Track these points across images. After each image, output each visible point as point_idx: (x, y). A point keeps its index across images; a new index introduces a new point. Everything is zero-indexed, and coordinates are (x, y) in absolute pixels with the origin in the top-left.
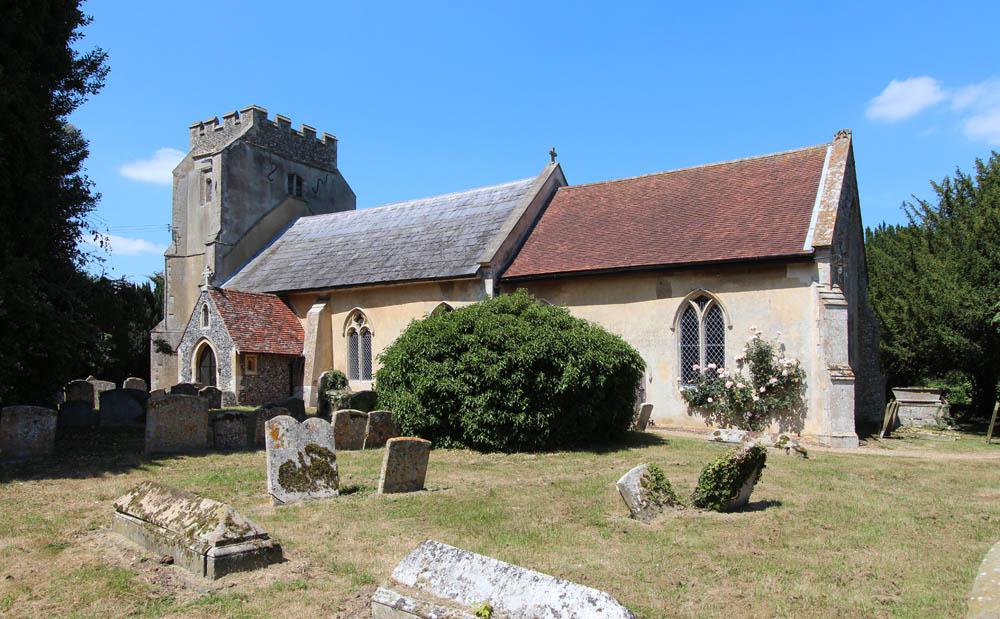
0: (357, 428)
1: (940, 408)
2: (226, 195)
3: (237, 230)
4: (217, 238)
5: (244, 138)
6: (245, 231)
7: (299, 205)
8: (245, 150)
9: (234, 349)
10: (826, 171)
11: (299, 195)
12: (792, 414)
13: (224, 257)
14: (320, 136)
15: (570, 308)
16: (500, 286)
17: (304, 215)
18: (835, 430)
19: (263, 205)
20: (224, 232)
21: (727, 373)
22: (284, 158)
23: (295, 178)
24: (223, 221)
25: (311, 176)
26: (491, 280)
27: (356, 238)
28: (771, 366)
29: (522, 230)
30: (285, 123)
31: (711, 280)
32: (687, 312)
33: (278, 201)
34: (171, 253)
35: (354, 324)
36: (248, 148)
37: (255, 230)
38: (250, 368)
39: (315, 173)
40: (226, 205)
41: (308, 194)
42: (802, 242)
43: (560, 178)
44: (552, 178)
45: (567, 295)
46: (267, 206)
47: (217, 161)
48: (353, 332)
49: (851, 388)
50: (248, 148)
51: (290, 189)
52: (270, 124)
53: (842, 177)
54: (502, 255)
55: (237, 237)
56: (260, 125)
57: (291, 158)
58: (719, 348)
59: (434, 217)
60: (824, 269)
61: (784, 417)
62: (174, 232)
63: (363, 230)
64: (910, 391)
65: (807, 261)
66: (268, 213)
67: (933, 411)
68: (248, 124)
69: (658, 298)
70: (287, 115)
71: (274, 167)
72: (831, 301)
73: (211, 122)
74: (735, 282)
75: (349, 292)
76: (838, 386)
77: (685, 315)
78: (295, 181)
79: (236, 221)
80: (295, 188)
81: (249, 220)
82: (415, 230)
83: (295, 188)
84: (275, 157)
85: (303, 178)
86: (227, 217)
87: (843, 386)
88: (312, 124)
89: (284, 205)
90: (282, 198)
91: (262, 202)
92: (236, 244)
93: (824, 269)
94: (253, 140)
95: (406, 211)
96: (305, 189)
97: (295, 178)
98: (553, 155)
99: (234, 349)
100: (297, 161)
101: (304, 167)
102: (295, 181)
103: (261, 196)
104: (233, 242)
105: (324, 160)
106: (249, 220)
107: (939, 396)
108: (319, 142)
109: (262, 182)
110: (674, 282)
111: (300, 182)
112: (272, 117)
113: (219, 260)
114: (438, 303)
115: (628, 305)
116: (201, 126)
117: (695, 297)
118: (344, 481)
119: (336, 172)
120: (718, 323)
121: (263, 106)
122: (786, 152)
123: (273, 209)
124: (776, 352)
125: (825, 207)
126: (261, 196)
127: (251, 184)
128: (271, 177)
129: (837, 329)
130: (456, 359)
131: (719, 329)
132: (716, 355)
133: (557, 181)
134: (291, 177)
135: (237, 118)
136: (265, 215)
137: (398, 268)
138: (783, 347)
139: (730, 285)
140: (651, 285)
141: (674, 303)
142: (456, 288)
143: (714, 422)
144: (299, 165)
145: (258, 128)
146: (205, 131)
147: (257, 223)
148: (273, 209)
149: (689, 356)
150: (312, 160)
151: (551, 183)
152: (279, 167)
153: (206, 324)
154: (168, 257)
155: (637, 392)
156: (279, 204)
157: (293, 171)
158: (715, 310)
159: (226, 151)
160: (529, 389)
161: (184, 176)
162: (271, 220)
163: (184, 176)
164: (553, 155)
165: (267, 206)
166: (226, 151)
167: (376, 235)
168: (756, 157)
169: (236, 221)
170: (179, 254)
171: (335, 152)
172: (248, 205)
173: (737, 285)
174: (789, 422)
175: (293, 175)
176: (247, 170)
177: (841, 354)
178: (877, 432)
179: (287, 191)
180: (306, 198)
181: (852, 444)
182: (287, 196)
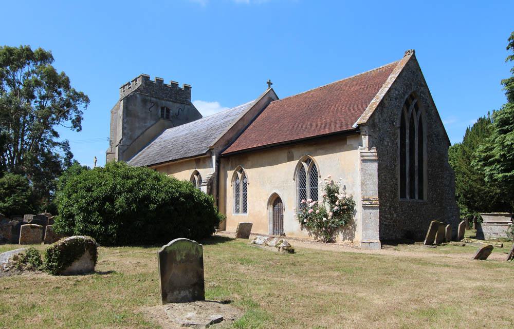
0: (36, 234)
1: (510, 226)
2: (125, 120)
3: (131, 138)
4: (120, 143)
5: (136, 91)
7: (166, 123)
8: (136, 97)
11: (168, 118)
12: (349, 229)
14: (181, 86)
17: (170, 127)
18: (365, 238)
19: (146, 124)
20: (124, 140)
22: (159, 99)
23: (165, 108)
24: (123, 134)
25: (174, 108)
26: (215, 156)
29: (240, 127)
30: (160, 81)
31: (311, 149)
32: (300, 168)
33: (154, 122)
34: (108, 152)
36: (138, 96)
37: (141, 137)
39: (177, 105)
40: (125, 125)
41: (172, 117)
43: (273, 97)
44: (267, 96)
45: (249, 163)
46: (148, 124)
49: (377, 212)
50: (138, 96)
51: (162, 115)
52: (152, 82)
54: (223, 142)
55: (131, 141)
56: (146, 84)
57: (163, 99)
60: (365, 140)
61: (345, 231)
62: (111, 141)
64: (488, 215)
65: (356, 133)
66: (149, 128)
67: (505, 228)
69: (288, 161)
70: (160, 76)
71: (153, 104)
72: (366, 158)
73: (127, 85)
74: (322, 149)
75: (162, 167)
76: (368, 211)
77: (301, 170)
79: (130, 133)
84: (154, 99)
86: (125, 131)
87: (371, 211)
88: (176, 80)
89: (158, 124)
90: (157, 120)
91: (145, 123)
92: (130, 145)
93: (365, 140)
94: (141, 91)
96: (171, 115)
97: (165, 108)
98: (270, 84)
100: (167, 100)
101: (171, 103)
103: (145, 119)
104: (129, 144)
105: (183, 98)
106: (138, 132)
107: (510, 218)
108: (180, 89)
109: (146, 112)
110: (295, 152)
111: (168, 111)
112: (153, 79)
113: (120, 154)
114: (194, 170)
115: (274, 166)
116: (124, 87)
117: (305, 159)
121: (147, 73)
122: (379, 68)
123: (152, 126)
124: (341, 190)
126: (145, 119)
127: (139, 114)
129: (370, 175)
132: (315, 196)
133: (271, 97)
134: (163, 109)
136: (146, 130)
138: (345, 188)
139: (321, 151)
140: (284, 154)
141: (295, 163)
142: (201, 162)
143: (312, 234)
144: (168, 102)
145: (144, 85)
147: (142, 134)
149: (303, 195)
151: (266, 100)
152: (156, 104)
154: (108, 154)
156: (155, 123)
157: (164, 105)
158: (313, 168)
160: (102, 211)
161: (115, 113)
162: (150, 132)
163: (115, 113)
164: (270, 84)
165: (148, 124)
168: (363, 73)
169: (130, 133)
170: (112, 152)
173: (323, 151)
174: (348, 234)
175: (164, 107)
176: (137, 107)
177: (373, 191)
178: (422, 240)
179: (160, 116)
180: (171, 119)
181: (377, 249)
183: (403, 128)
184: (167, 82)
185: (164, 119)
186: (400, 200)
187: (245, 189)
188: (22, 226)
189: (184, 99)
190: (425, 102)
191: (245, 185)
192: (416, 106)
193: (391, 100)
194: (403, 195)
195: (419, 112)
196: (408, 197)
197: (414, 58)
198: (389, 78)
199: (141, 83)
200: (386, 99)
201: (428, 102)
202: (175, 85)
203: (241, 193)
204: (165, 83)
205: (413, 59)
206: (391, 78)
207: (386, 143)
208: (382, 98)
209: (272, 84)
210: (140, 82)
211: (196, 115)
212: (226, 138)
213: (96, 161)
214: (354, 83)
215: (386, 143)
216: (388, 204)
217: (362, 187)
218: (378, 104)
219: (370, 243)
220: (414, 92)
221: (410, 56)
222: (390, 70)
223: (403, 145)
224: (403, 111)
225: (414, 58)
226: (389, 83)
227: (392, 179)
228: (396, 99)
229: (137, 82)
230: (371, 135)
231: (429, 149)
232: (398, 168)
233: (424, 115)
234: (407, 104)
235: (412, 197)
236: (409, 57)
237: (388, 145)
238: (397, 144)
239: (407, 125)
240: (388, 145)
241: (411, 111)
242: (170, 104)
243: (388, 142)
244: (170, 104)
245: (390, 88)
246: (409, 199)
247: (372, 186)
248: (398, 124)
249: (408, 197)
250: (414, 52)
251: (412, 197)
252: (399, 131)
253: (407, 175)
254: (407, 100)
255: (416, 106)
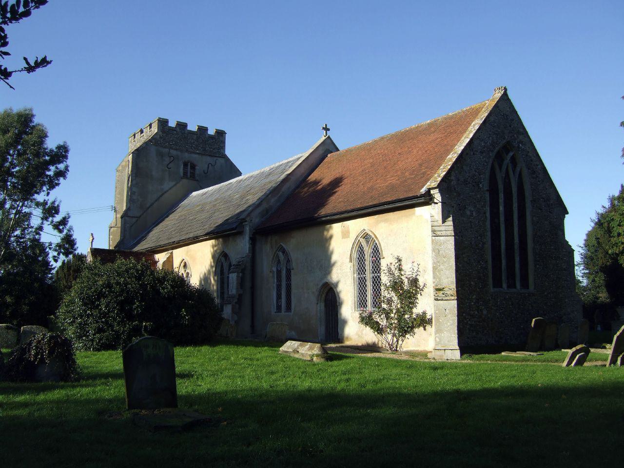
6: (148, 206)
11: (193, 177)
21: (384, 281)
23: (189, 164)
25: (202, 163)
28: (52, 151)
30: (182, 126)
39: (209, 159)
51: (185, 174)
78: (189, 167)
86: (135, 197)
92: (140, 216)
96: (197, 172)
97: (189, 164)
98: (326, 129)
100: (191, 153)
102: (189, 167)
111: (193, 167)
112: (172, 124)
118: (36, 59)
128: (169, 166)
133: (328, 147)
134: (185, 165)
145: (161, 133)
151: (321, 152)
155: (338, 304)
183: (493, 190)
184: (192, 127)
185: (187, 178)
186: (492, 290)
187: (289, 278)
188: (534, 320)
189: (216, 150)
190: (527, 155)
191: (289, 272)
192: (513, 159)
193: (474, 154)
194: (497, 283)
195: (518, 169)
196: (505, 285)
197: (506, 98)
198: (472, 124)
199: (156, 131)
200: (467, 154)
201: (530, 154)
202: (203, 130)
203: (369, 276)
204: (189, 128)
205: (505, 98)
206: (474, 125)
207: (468, 213)
208: (460, 152)
209: (328, 130)
210: (155, 129)
211: (234, 172)
212: (265, 206)
213: (93, 239)
214: (432, 129)
215: (468, 213)
216: (474, 297)
217: (434, 273)
218: (454, 160)
219: (445, 350)
220: (508, 143)
221: (500, 95)
222: (475, 113)
223: (495, 214)
224: (493, 169)
225: (506, 98)
226: (471, 131)
227: (479, 262)
228: (482, 153)
229: (152, 129)
230: (445, 203)
231: (534, 218)
232: (488, 246)
233: (525, 172)
234: (499, 157)
235: (511, 285)
236: (498, 95)
237: (472, 215)
238: (485, 213)
239: (501, 187)
240: (472, 215)
241: (504, 169)
242: (195, 158)
243: (471, 211)
244: (195, 158)
245: (472, 139)
246: (506, 289)
247: (447, 272)
248: (485, 185)
249: (505, 285)
250: (505, 89)
251: (511, 285)
252: (487, 195)
253: (503, 256)
254: (498, 152)
255: (513, 159)
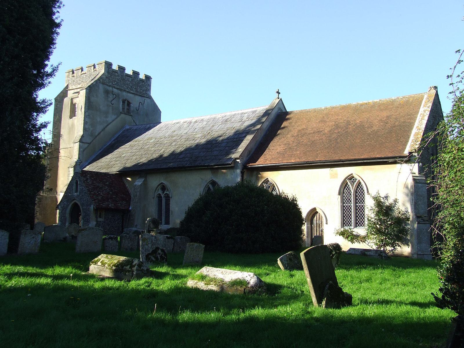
9: (92, 206)
10: (422, 110)
13: (84, 151)
15: (445, 115)
16: (245, 170)
19: (107, 119)
24: (85, 129)
27: (162, 140)
35: (160, 192)
38: (100, 217)
39: (138, 99)
42: (404, 149)
47: (83, 93)
48: (159, 197)
51: (123, 109)
53: (429, 113)
56: (108, 72)
58: (362, 206)
59: (208, 128)
63: (167, 135)
68: (101, 71)
80: (126, 109)
81: (99, 128)
82: (198, 136)
83: (126, 109)
84: (115, 90)
85: (131, 101)
89: (119, 119)
91: (106, 117)
95: (192, 124)
96: (132, 109)
99: (92, 206)
101: (131, 95)
104: (89, 142)
111: (129, 104)
112: (115, 67)
119: (150, 98)
120: (362, 192)
123: (113, 121)
125: (418, 130)
130: (435, 135)
131: (362, 196)
134: (124, 102)
135: (95, 68)
137: (187, 159)
145: (107, 74)
146: (75, 75)
148: (113, 121)
150: (137, 91)
153: (76, 192)
159: (88, 89)
166: (88, 89)
167: (174, 138)
169: (91, 129)
171: (150, 86)
172: (99, 120)
176: (100, 98)
179: (121, 110)
182: (121, 113)
